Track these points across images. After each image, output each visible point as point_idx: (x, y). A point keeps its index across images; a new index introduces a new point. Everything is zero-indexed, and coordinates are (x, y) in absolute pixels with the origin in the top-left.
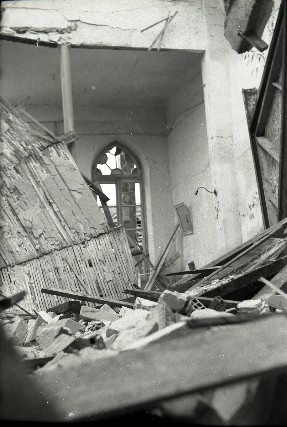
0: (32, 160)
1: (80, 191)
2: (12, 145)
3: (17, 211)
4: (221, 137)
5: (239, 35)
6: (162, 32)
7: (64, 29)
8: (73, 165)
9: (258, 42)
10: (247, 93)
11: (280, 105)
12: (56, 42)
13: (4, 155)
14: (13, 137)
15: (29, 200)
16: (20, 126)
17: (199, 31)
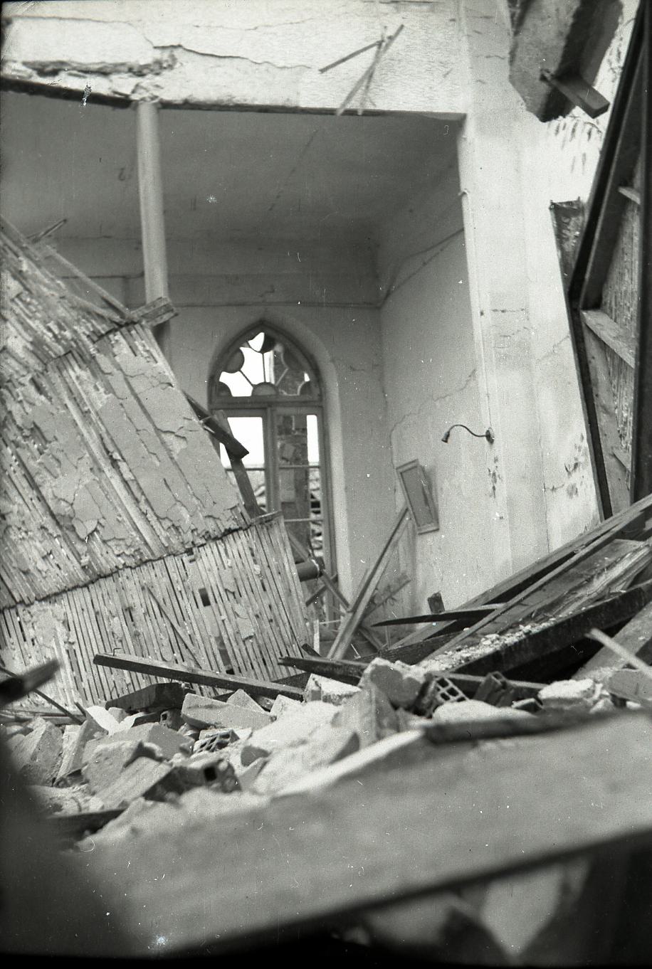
0: (73, 362)
1: (182, 433)
2: (27, 328)
3: (38, 479)
4: (503, 311)
5: (543, 78)
6: (367, 72)
7: (146, 66)
8: (167, 374)
9: (585, 96)
10: (561, 212)
11: (636, 239)
12: (127, 96)
13: (8, 352)
14: (30, 310)
15: (66, 454)
16: (45, 285)
17: (452, 70)
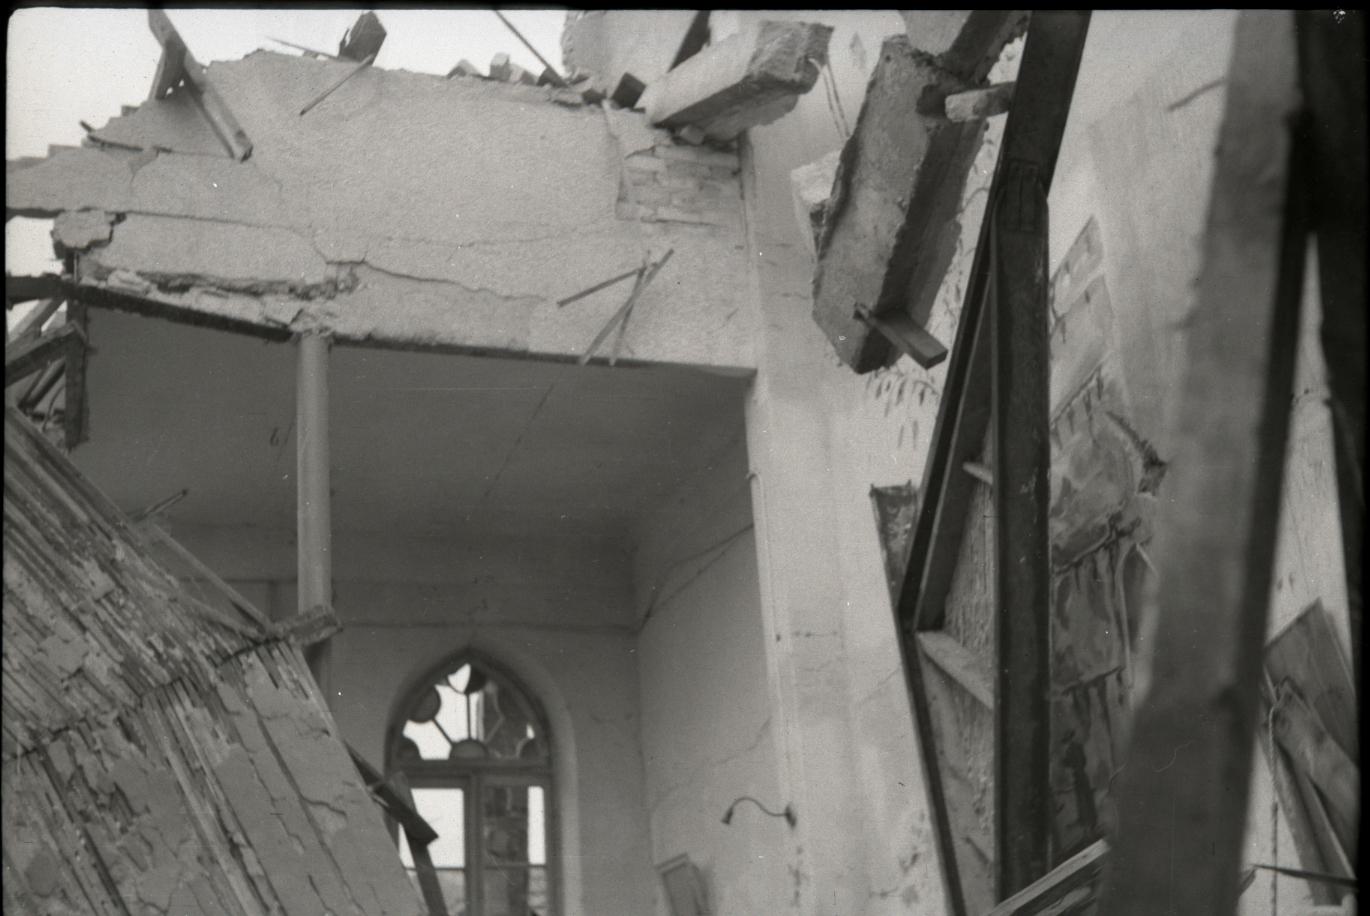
0: (182, 694)
1: (339, 805)
2: (117, 642)
3: (115, 873)
4: (808, 635)
5: (858, 316)
6: (621, 310)
7: (316, 287)
8: (322, 715)
9: (913, 339)
10: (885, 500)
11: (990, 532)
12: (285, 326)
13: (86, 678)
14: (124, 617)
15: (161, 835)
16: (150, 582)
17: (737, 310)
